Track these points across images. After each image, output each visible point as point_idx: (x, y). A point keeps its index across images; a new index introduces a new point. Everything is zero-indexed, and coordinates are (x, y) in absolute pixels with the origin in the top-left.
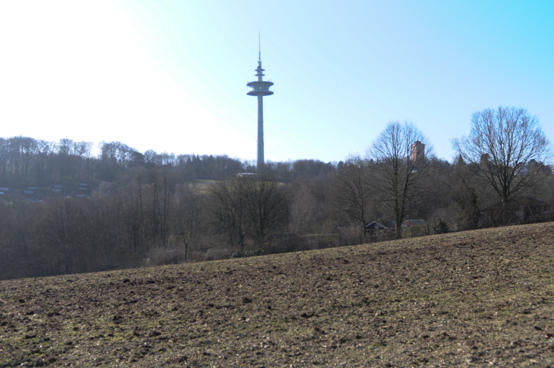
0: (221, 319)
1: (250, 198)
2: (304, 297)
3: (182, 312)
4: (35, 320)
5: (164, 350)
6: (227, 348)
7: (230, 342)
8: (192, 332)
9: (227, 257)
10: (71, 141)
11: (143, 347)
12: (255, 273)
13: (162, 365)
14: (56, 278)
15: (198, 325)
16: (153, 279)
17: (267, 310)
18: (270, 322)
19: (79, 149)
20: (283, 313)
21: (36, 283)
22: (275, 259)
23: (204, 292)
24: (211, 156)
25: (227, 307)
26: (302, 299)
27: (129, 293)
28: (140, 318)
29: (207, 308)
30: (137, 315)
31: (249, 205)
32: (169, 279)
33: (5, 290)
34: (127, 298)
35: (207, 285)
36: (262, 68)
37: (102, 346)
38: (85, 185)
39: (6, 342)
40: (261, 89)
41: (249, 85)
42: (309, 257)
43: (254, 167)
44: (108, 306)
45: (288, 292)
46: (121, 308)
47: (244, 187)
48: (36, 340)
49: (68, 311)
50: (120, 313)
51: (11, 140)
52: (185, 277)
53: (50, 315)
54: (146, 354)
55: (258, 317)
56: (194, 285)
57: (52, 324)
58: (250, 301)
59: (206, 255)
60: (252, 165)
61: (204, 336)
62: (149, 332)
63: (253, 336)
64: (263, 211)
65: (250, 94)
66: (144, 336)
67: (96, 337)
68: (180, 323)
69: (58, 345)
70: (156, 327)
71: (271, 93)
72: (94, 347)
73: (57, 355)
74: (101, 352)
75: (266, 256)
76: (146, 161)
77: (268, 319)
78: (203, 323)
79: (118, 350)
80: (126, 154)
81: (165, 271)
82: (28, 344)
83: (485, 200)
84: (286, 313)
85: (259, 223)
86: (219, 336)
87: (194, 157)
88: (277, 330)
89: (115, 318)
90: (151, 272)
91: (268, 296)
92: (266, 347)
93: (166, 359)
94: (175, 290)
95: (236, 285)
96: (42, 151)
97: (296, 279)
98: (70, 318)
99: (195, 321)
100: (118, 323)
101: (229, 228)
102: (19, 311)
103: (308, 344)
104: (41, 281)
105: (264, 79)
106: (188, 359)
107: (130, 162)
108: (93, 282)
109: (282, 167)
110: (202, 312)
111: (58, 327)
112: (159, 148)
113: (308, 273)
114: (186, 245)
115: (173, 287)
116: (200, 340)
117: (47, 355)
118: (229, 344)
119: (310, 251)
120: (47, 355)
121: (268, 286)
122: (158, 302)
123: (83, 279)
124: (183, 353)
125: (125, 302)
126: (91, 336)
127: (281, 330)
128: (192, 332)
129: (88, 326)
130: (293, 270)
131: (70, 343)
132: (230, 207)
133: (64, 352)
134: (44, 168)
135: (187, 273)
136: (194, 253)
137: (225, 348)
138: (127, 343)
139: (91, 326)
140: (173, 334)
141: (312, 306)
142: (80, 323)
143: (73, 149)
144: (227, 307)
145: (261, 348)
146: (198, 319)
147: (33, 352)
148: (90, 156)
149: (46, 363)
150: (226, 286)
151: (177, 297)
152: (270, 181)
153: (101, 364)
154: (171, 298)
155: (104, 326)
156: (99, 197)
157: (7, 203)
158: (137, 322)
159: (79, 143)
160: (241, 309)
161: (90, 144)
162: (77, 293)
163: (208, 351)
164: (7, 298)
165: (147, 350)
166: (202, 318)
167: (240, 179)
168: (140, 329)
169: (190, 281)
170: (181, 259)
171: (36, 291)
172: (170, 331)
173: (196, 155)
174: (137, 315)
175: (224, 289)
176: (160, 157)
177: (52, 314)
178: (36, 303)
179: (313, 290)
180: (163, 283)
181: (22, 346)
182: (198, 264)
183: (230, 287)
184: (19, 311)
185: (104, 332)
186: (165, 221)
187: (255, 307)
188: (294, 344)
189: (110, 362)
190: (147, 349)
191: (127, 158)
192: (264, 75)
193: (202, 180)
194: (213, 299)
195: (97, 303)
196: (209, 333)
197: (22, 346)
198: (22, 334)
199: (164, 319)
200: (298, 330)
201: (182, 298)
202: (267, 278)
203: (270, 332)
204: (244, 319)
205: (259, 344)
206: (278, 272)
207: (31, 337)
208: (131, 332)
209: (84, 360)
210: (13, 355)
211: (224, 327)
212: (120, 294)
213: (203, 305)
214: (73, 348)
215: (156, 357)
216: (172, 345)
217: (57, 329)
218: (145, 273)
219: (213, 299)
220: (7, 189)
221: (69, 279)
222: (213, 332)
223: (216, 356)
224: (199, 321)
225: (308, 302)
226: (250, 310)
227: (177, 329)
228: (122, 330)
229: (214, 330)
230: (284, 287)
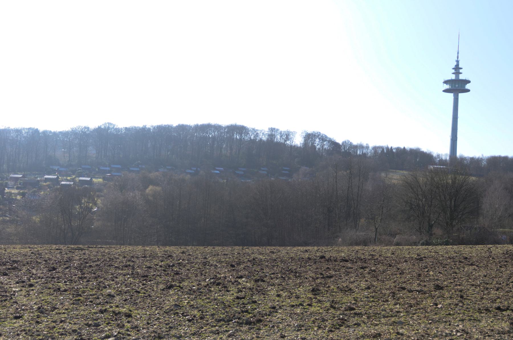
0: (413, 302)
1: (441, 190)
2: (497, 290)
3: (374, 291)
4: (244, 283)
5: (358, 325)
6: (420, 331)
7: (423, 325)
8: (385, 311)
9: (415, 244)
10: (278, 130)
11: (339, 319)
12: (445, 262)
13: (357, 338)
14: (261, 249)
15: (390, 305)
16: (347, 258)
17: (459, 299)
18: (462, 311)
19: (284, 137)
20: (476, 304)
21: (244, 252)
22: (466, 250)
23: (396, 274)
24: (404, 148)
25: (419, 292)
26: (496, 292)
27: (325, 268)
28: (336, 292)
29: (399, 291)
30: (333, 289)
31: (440, 197)
32: (362, 260)
33: (218, 255)
34: (324, 273)
35: (398, 269)
36: (460, 66)
37: (302, 313)
38: (288, 169)
39: (221, 300)
40: (457, 86)
41: (446, 82)
42: (501, 252)
43: (446, 160)
44: (306, 278)
45: (480, 283)
46: (319, 281)
47: (436, 179)
48: (245, 301)
49: (272, 279)
50: (317, 286)
51: (228, 127)
52: (377, 259)
53: (256, 281)
54: (342, 326)
55: (450, 304)
56: (385, 268)
57: (258, 289)
58: (442, 288)
59: (395, 240)
60: (444, 158)
61: (396, 316)
62: (344, 306)
63: (446, 322)
64: (453, 203)
65: (446, 91)
66: (340, 310)
67: (296, 305)
68: (373, 301)
69: (264, 308)
70: (351, 303)
71: (468, 91)
72: (296, 314)
73: (263, 317)
74: (301, 319)
75: (455, 247)
76: (343, 150)
77: (460, 308)
78: (395, 304)
79: (316, 319)
80: (325, 143)
81: (357, 251)
82: (239, 304)
83: (447, 203)
84: (479, 304)
85: (449, 215)
86: (411, 318)
87: (387, 148)
88: (470, 320)
89: (313, 290)
90: (345, 251)
91: (460, 285)
92: (459, 334)
93: (361, 333)
94: (368, 270)
95: (427, 271)
96: (252, 137)
97: (488, 272)
98: (273, 285)
99: (388, 301)
100: (315, 295)
101: (418, 216)
102: (230, 274)
103: (503, 337)
104: (248, 250)
105: (461, 77)
106: (382, 336)
107: (328, 150)
108: (292, 255)
109: (475, 162)
110: (394, 293)
111: (263, 292)
112: (356, 139)
113: (500, 267)
114: (376, 229)
115: (366, 267)
116: (393, 319)
117: (254, 316)
118: (422, 327)
119: (502, 246)
120: (254, 316)
121: (459, 275)
122: (352, 280)
123: (284, 251)
124: (376, 330)
125: (322, 276)
126: (292, 303)
127: (474, 320)
128: (385, 311)
129: (289, 294)
130: (485, 263)
131: (274, 308)
132: (420, 197)
133: (269, 315)
134: (254, 152)
135: (378, 255)
136: (383, 237)
137: (418, 330)
138: (324, 313)
139: (292, 294)
140: (367, 311)
141: (507, 300)
142: (282, 290)
143: (279, 137)
144: (419, 292)
145: (453, 335)
146: (390, 300)
147: (243, 312)
148: (293, 144)
149: (254, 323)
150: (417, 271)
151: (369, 277)
152: (462, 175)
153: (301, 330)
154: (365, 277)
155: (303, 296)
156: (300, 180)
157: (221, 181)
158: (333, 295)
159: (284, 132)
160: (433, 295)
161: (294, 133)
162: (279, 263)
163: (401, 331)
164: (220, 262)
165: (343, 323)
166: (394, 299)
167: (431, 171)
168: (336, 303)
169: (382, 263)
170: (370, 242)
171: (244, 258)
172: (364, 308)
173: (390, 147)
174: (333, 289)
175: (415, 274)
176: (356, 147)
177: (259, 280)
178: (244, 269)
179: (507, 285)
180: (356, 262)
181: (234, 305)
182: (388, 247)
183: (421, 272)
184: (230, 274)
185: (304, 301)
186: (357, 205)
187: (447, 295)
188: (489, 336)
189: (309, 329)
190: (343, 322)
191: (326, 147)
192: (461, 73)
193: (395, 171)
194: (405, 282)
195: (297, 275)
196: (402, 314)
197: (234, 305)
198: (233, 294)
199: (358, 296)
200: (492, 322)
201: (375, 279)
202: (458, 268)
203: (462, 320)
204: (436, 305)
205: (452, 331)
206: (470, 263)
207: (241, 298)
208: (328, 304)
209: (286, 324)
210: (227, 312)
211: (416, 310)
212: (317, 268)
213: (395, 287)
214: (277, 312)
215: (351, 330)
216: (366, 321)
217: (263, 294)
218: (339, 252)
219: (405, 282)
220: (222, 169)
221: (272, 251)
222: (405, 314)
223: (409, 337)
224: (391, 301)
225: (502, 296)
226: (442, 296)
227: (371, 307)
228: (320, 301)
229: (407, 312)
230: (476, 279)
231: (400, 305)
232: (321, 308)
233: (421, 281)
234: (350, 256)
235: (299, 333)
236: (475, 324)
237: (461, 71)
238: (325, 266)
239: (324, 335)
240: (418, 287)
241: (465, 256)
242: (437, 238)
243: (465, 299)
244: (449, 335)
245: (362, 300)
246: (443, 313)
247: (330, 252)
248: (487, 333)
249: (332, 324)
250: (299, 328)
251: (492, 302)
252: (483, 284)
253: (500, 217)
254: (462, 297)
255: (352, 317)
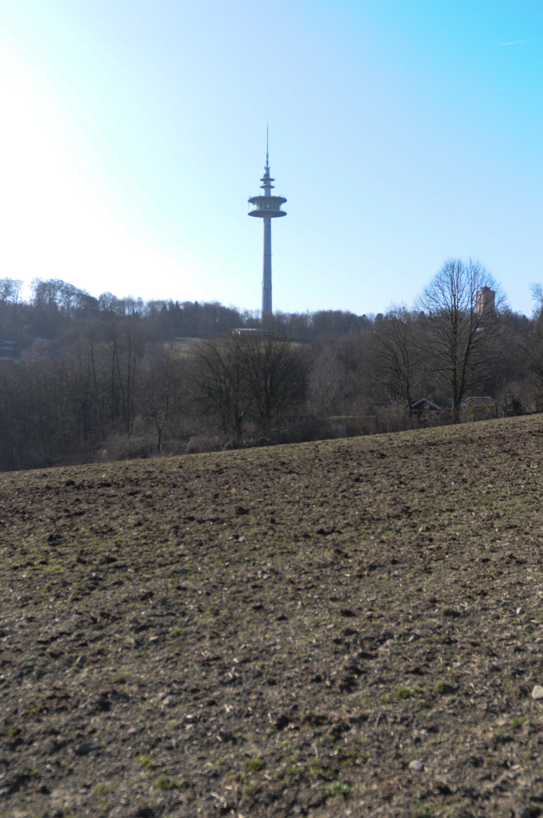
0: (204, 537)
1: (251, 365)
2: (322, 505)
3: (148, 529)
5: (120, 583)
6: (211, 580)
7: (216, 570)
8: (162, 556)
9: (218, 448)
11: (90, 579)
12: (255, 472)
15: (172, 546)
16: (110, 481)
17: (270, 524)
18: (272, 542)
20: (291, 529)
23: (182, 498)
24: (196, 303)
25: (214, 520)
26: (319, 509)
27: (72, 501)
28: (88, 537)
29: (184, 523)
30: (84, 533)
31: (250, 375)
32: (132, 481)
34: (70, 508)
35: (186, 490)
36: (271, 176)
37: (30, 578)
38: (12, 342)
40: (268, 207)
41: (252, 200)
42: (331, 449)
43: (257, 320)
47: (242, 349)
50: (59, 530)
52: (156, 477)
54: (94, 589)
55: (256, 534)
56: (167, 490)
58: (246, 512)
59: (189, 445)
60: (254, 317)
61: (178, 562)
62: (99, 557)
63: (249, 561)
65: (253, 214)
68: (145, 544)
70: (110, 551)
71: (284, 214)
72: (19, 580)
74: (29, 587)
75: (272, 447)
76: (102, 309)
77: (270, 537)
78: (179, 544)
79: (53, 584)
80: (72, 298)
81: (127, 468)
83: (460, 367)
84: (296, 529)
85: (264, 401)
86: (200, 562)
87: (171, 304)
88: (282, 553)
89: (51, 538)
90: (107, 470)
91: (271, 504)
92: (265, 577)
93: (123, 596)
94: (139, 496)
95: (228, 489)
97: (312, 481)
99: (167, 540)
100: (54, 545)
105: (274, 193)
107: (78, 310)
108: (21, 485)
109: (298, 321)
110: (177, 528)
113: (328, 472)
114: (160, 431)
115: (137, 492)
116: (173, 568)
118: (214, 573)
119: (333, 440)
121: (272, 490)
122: (114, 514)
125: (67, 514)
127: (288, 552)
128: (162, 556)
129: (11, 550)
132: (222, 377)
135: (158, 471)
137: (208, 579)
138: (67, 572)
139: (15, 549)
140: (134, 560)
141: (332, 518)
144: (214, 520)
145: (258, 579)
146: (171, 539)
148: (19, 301)
150: (213, 490)
151: (142, 507)
152: (280, 340)
153: (28, 604)
154: (134, 508)
156: (33, 360)
158: (83, 543)
161: (19, 283)
163: (183, 584)
167: (236, 337)
169: (163, 483)
170: (152, 451)
172: (131, 556)
174: (84, 533)
175: (210, 495)
179: (335, 496)
180: (123, 486)
183: (219, 491)
185: (34, 559)
186: (129, 396)
189: (41, 602)
192: (273, 187)
193: (184, 338)
194: (194, 509)
195: (25, 515)
196: (187, 558)
199: (122, 539)
200: (311, 552)
202: (271, 480)
203: (272, 555)
204: (237, 537)
205: (256, 574)
206: (288, 471)
208: (74, 558)
211: (208, 549)
215: (109, 593)
216: (132, 576)
218: (98, 471)
219: (194, 509)
222: (191, 557)
223: (195, 591)
224: (173, 540)
226: (246, 524)
227: (141, 553)
228: (61, 555)
229: (194, 554)
230: (294, 493)
231: (185, 544)
232: (63, 566)
233: (217, 505)
234: (115, 477)
235: (23, 610)
236: (289, 559)
237: (272, 184)
238: (73, 496)
239: (65, 608)
240: (213, 514)
241: (283, 460)
242: (249, 437)
243: (277, 524)
244: (251, 580)
245: (129, 543)
246: (245, 549)
247: (82, 472)
248: (304, 569)
249: (79, 589)
250: (24, 603)
251: (314, 524)
252: (303, 499)
253: (334, 399)
254: (273, 521)
255: (111, 573)
